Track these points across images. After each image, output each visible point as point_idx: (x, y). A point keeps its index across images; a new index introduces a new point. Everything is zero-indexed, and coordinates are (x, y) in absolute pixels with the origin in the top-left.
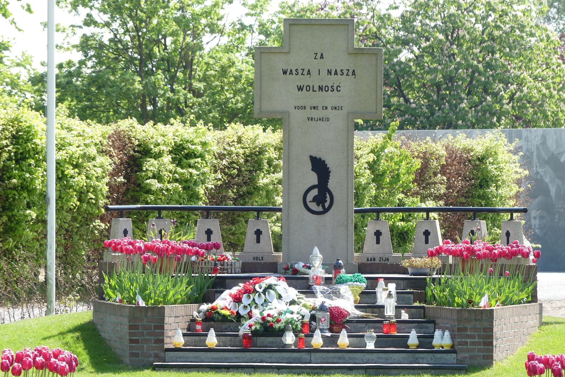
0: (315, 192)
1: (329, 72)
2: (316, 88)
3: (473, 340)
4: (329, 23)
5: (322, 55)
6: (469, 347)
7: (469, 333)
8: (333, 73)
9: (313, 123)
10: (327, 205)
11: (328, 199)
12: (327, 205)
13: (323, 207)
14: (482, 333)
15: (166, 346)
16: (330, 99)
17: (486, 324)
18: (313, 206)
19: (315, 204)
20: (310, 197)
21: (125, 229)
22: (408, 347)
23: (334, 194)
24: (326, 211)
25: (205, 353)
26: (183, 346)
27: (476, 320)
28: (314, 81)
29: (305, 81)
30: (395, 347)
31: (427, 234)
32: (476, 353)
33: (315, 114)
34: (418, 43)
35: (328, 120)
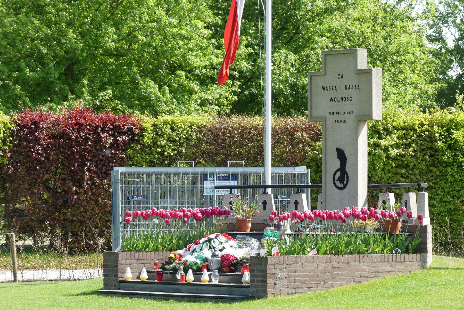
0: (339, 174)
1: (346, 87)
2: (339, 100)
3: (258, 279)
4: (345, 52)
5: (342, 76)
6: (256, 283)
7: (255, 274)
8: (348, 88)
9: (338, 124)
10: (345, 182)
11: (346, 178)
12: (345, 182)
13: (343, 184)
14: (262, 274)
15: (120, 279)
16: (346, 106)
17: (263, 267)
18: (338, 183)
19: (339, 182)
20: (336, 178)
21: (296, 201)
22: (242, 283)
23: (349, 175)
24: (345, 186)
25: (239, 288)
26: (193, 281)
27: (259, 264)
28: (338, 94)
29: (333, 94)
30: (235, 283)
31: (265, 203)
32: (259, 289)
33: (340, 117)
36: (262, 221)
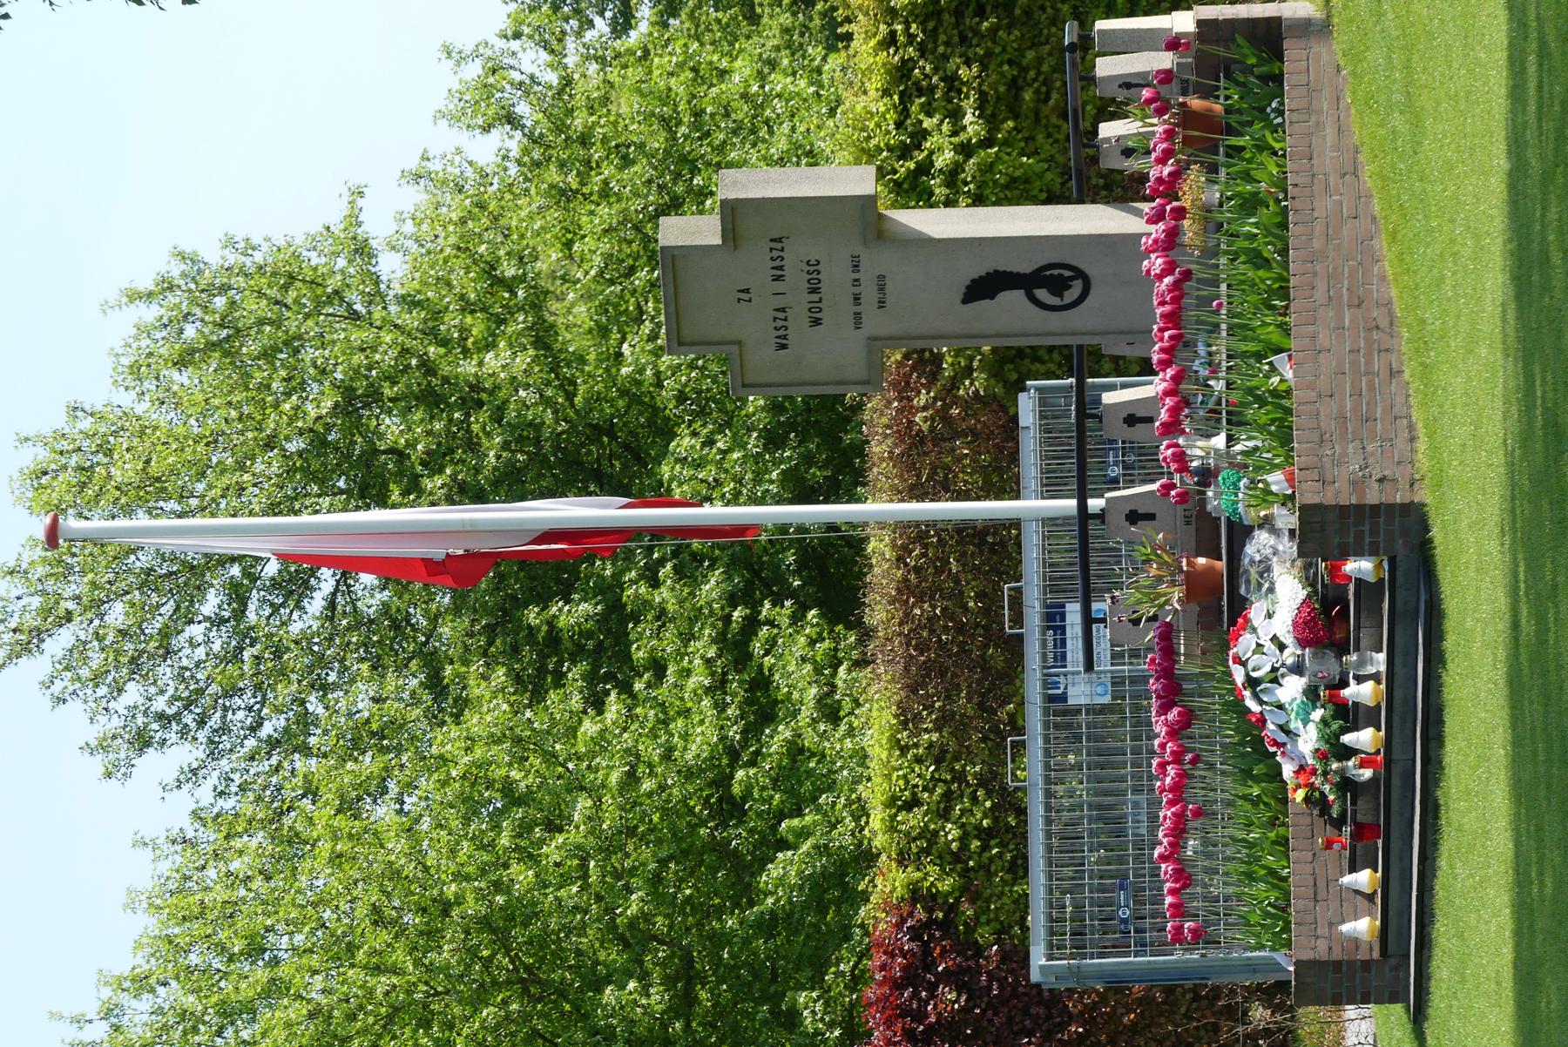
0: (1042, 294)
2: (815, 297)
7: (1351, 540)
9: (890, 300)
10: (1067, 273)
11: (1056, 272)
12: (1067, 273)
15: (1376, 955)
16: (835, 277)
18: (1072, 294)
20: (1055, 301)
24: (1080, 274)
26: (1379, 729)
27: (1323, 530)
28: (799, 302)
30: (1382, 601)
33: (870, 294)
34: (710, 938)
35: (881, 277)
36: (1188, 523)
